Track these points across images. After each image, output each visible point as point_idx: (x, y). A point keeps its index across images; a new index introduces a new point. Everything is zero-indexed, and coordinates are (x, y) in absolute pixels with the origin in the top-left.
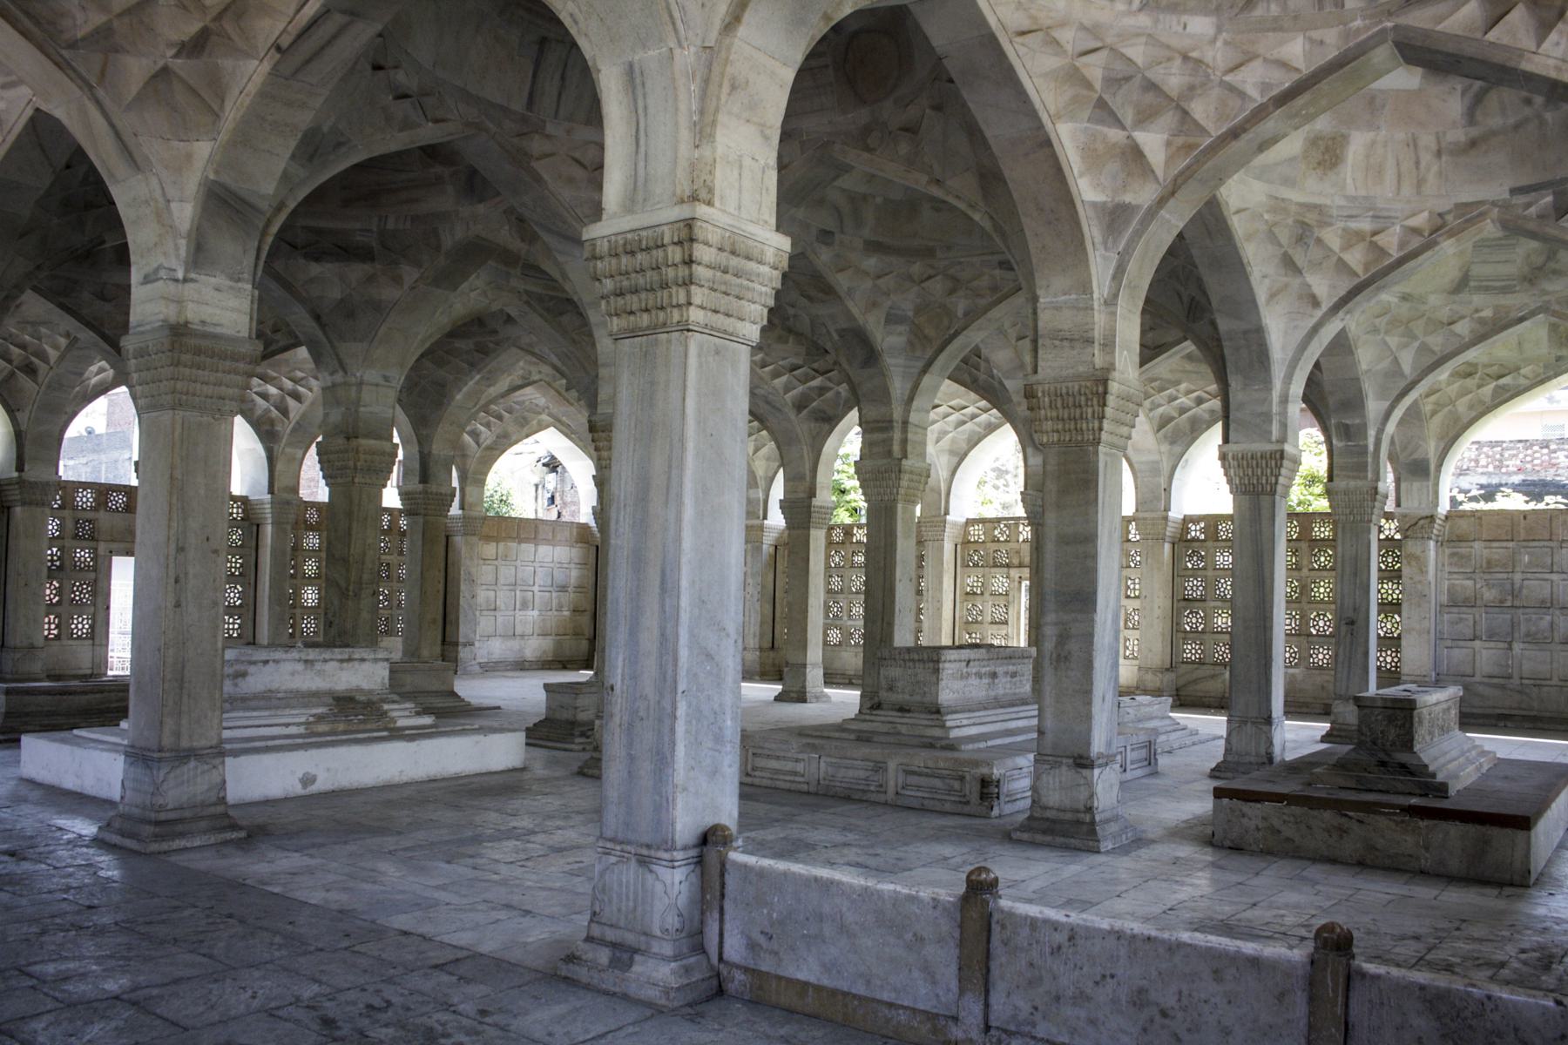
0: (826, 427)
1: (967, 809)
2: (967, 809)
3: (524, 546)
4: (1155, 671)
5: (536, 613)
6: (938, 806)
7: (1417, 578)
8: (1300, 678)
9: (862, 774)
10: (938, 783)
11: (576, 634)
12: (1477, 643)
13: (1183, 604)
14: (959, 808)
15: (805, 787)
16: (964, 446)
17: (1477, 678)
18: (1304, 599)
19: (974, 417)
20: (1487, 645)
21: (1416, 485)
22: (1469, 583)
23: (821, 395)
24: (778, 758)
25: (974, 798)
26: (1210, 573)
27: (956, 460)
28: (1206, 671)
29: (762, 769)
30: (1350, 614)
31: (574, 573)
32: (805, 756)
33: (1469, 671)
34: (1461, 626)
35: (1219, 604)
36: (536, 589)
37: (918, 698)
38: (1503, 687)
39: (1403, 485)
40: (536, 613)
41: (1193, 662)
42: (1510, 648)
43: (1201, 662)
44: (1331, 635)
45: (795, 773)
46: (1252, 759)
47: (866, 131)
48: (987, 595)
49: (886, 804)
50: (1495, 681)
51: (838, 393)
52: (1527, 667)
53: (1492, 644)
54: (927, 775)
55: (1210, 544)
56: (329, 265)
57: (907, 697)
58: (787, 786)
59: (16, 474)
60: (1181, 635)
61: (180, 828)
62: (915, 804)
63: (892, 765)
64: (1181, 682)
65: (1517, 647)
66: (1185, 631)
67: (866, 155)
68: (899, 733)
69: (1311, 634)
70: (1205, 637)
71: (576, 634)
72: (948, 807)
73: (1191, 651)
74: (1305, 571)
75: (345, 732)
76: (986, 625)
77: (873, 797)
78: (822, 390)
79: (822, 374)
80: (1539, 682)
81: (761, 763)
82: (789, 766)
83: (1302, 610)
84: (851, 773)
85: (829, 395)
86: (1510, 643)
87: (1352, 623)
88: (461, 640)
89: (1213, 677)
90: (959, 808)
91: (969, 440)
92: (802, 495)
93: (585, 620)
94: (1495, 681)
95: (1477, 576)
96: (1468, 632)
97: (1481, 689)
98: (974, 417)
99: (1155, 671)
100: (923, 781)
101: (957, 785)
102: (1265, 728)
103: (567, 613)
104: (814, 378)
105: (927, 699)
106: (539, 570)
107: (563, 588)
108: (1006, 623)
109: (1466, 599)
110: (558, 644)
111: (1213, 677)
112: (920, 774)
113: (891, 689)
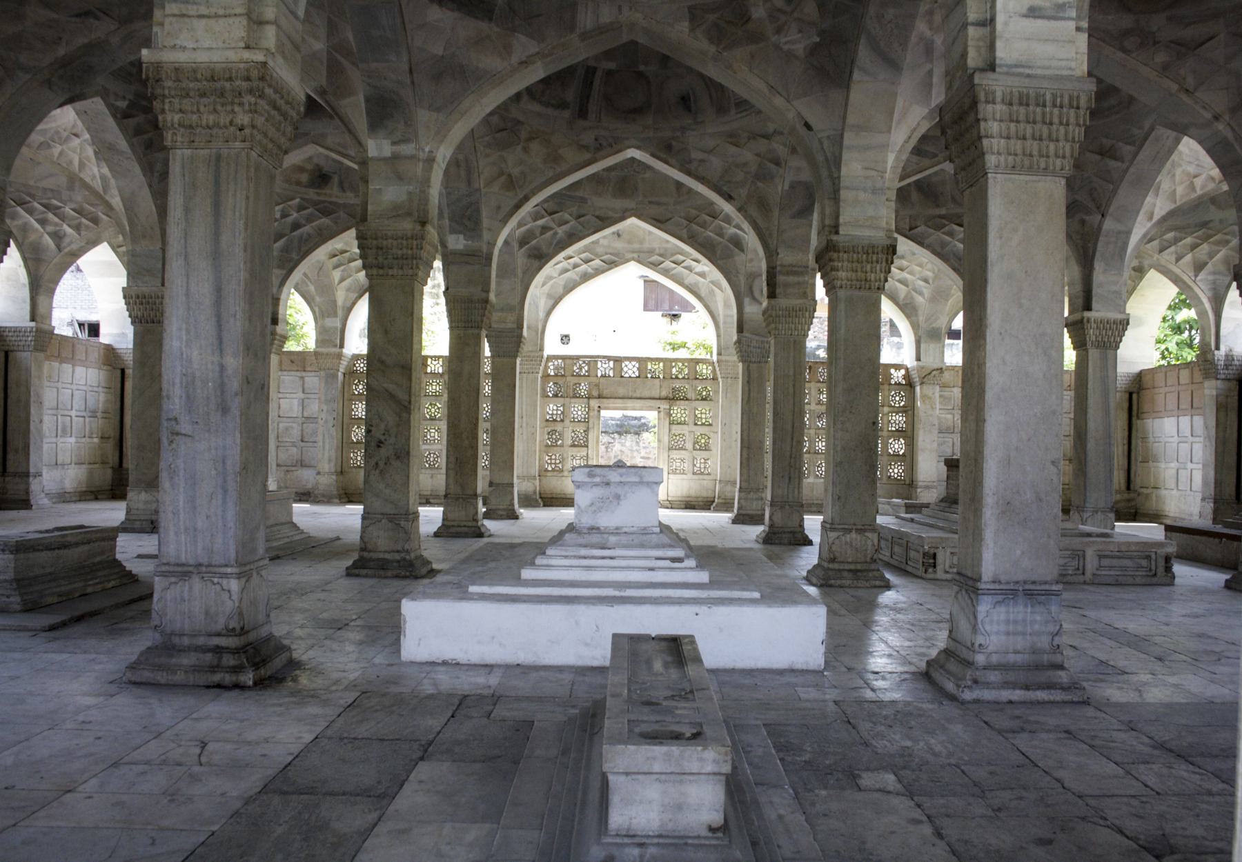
0: (536, 263)
1: (1155, 580)
3: (64, 365)
5: (73, 440)
6: (1130, 580)
11: (103, 463)
14: (1149, 581)
16: (561, 291)
19: (576, 266)
21: (932, 346)
22: (950, 416)
23: (542, 234)
25: (1161, 570)
27: (552, 302)
31: (102, 398)
36: (73, 413)
39: (923, 346)
40: (73, 440)
47: (1126, 33)
48: (567, 422)
51: (556, 234)
54: (1119, 558)
56: (449, 13)
59: (904, 245)
61: (1011, 677)
63: (1090, 553)
67: (1120, 54)
71: (103, 463)
72: (1138, 580)
76: (566, 448)
77: (1075, 579)
78: (545, 229)
79: (550, 214)
85: (549, 234)
88: (32, 470)
90: (1149, 581)
91: (565, 287)
92: (510, 325)
93: (110, 447)
98: (576, 266)
100: (1115, 562)
101: (1144, 563)
103: (96, 440)
104: (543, 217)
106: (76, 393)
107: (93, 414)
109: (948, 428)
110: (91, 474)
112: (1112, 557)
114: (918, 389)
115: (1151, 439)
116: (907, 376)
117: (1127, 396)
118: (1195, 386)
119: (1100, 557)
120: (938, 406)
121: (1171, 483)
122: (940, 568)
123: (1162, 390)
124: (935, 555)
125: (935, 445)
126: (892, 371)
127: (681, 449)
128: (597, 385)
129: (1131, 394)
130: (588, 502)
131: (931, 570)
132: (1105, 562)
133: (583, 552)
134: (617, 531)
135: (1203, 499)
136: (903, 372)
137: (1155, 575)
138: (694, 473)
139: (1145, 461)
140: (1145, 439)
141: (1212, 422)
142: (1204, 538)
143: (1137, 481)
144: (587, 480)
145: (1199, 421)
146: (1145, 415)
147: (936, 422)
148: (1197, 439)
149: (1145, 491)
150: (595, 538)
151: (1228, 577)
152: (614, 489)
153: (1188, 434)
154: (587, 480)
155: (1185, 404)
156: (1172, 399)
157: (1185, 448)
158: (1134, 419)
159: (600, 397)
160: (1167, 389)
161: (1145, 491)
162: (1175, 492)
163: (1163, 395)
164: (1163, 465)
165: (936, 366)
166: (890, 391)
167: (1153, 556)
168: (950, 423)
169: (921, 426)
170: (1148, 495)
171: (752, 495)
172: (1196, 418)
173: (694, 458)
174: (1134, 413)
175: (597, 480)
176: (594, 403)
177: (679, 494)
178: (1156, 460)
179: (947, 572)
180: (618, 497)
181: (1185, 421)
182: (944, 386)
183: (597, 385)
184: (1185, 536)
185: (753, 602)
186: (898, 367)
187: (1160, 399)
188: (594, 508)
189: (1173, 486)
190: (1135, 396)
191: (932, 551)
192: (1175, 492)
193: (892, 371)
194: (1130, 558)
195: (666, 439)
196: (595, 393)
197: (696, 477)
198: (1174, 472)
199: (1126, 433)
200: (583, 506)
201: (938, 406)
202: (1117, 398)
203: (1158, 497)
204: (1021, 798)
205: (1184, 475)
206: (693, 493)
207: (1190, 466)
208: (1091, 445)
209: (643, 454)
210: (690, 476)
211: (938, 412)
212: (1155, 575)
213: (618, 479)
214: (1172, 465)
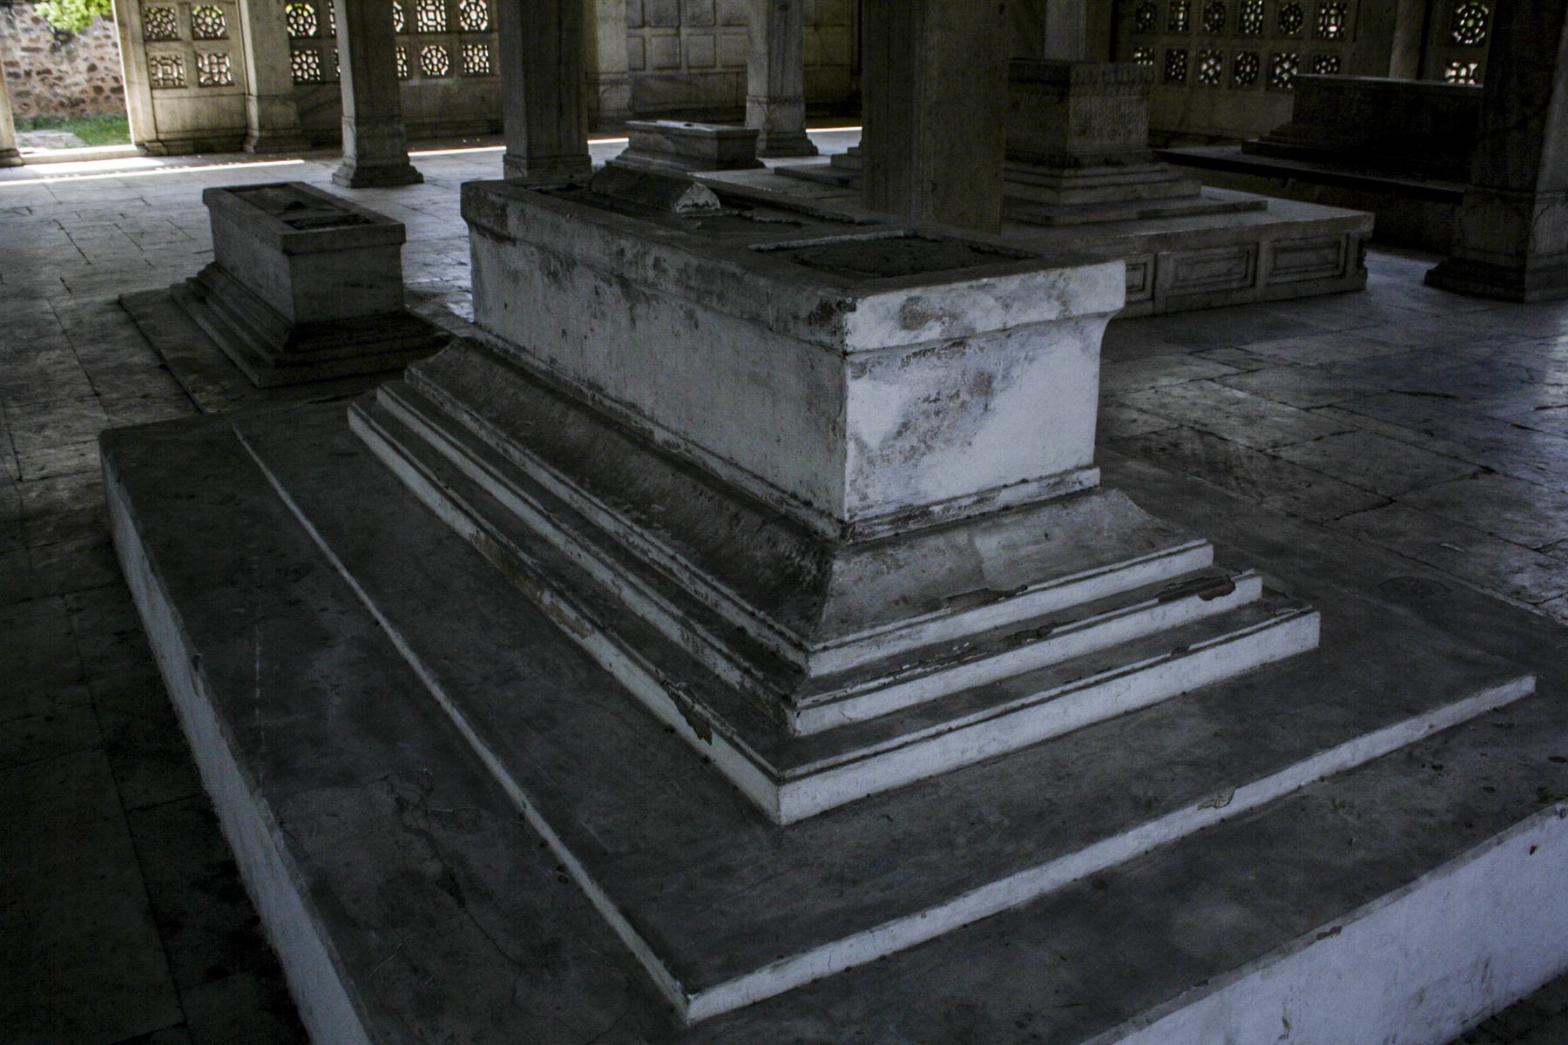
4: (285, 99)
8: (455, 89)
9: (1222, 267)
10: (1312, 257)
12: (647, 30)
17: (649, 72)
20: (656, 31)
38: (672, 79)
42: (678, 35)
44: (489, 30)
49: (1255, 303)
50: (665, 73)
52: (694, 53)
53: (661, 31)
54: (1301, 250)
63: (1265, 246)
65: (684, 31)
68: (1139, 200)
75: (1054, 572)
80: (705, 70)
86: (678, 28)
94: (665, 73)
97: (652, 83)
99: (285, 99)
101: (1330, 254)
113: (1083, 131)
127: (168, 38)
130: (888, 421)
132: (1285, 259)
133: (934, 631)
134: (985, 513)
137: (1344, 273)
138: (201, 85)
144: (901, 338)
150: (932, 560)
151: (1432, 266)
152: (976, 359)
154: (901, 338)
167: (1343, 243)
173: (197, 56)
175: (932, 332)
177: (178, 125)
180: (984, 385)
185: (1166, 660)
188: (910, 440)
194: (1315, 248)
195: (135, 21)
197: (206, 92)
200: (873, 442)
204: (890, 886)
206: (204, 122)
209: (25, 43)
210: (194, 90)
212: (1344, 273)
213: (995, 321)
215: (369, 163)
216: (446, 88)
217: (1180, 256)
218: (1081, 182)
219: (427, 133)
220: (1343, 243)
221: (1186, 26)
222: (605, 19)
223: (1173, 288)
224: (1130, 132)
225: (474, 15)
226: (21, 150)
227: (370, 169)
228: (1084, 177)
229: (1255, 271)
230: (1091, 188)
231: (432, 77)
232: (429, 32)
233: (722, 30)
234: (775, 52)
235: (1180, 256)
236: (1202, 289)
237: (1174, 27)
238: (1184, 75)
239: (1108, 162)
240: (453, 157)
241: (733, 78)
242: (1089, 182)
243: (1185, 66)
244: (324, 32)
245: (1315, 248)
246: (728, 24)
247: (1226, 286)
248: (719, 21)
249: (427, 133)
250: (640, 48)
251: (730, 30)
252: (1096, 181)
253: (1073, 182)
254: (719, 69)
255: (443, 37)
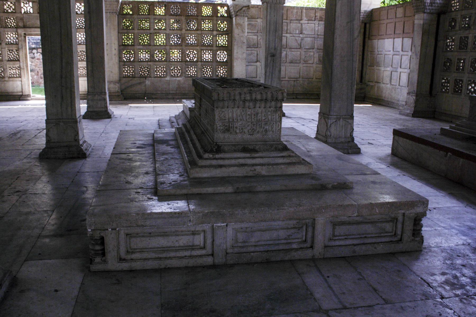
2: (399, 247)
6: (370, 250)
7: (241, 35)
8: (182, 81)
9: (282, 234)
10: (369, 229)
13: (122, 47)
15: (209, 260)
18: (184, 44)
22: (255, 37)
24: (165, 235)
25: (408, 235)
26: (136, 31)
28: (136, 81)
29: (142, 251)
30: (273, 51)
32: (207, 227)
33: (254, 75)
34: (252, 56)
35: (141, 47)
37: (258, 136)
41: (129, 77)
43: (133, 77)
45: (192, 247)
46: (343, 140)
54: (358, 223)
55: (135, 16)
57: (246, 137)
58: (184, 263)
60: (123, 63)
62: (346, 252)
63: (321, 221)
64: (123, 87)
66: (124, 61)
69: (187, 61)
70: (136, 64)
72: (380, 249)
73: (128, 71)
74: (184, 30)
76: (5, 62)
81: (138, 243)
82: (184, 240)
83: (182, 49)
84: (267, 236)
87: (273, 56)
89: (140, 83)
95: (259, 34)
96: (255, 59)
100: (353, 229)
101: (388, 227)
102: (350, 121)
105: (270, 135)
108: (19, 60)
111: (140, 83)
112: (349, 223)
113: (227, 130)
114: (234, 19)
115: (376, 52)
116: (228, 11)
117: (363, 25)
118: (406, 19)
119: (335, 225)
120: (246, 31)
121: (387, 80)
122: (111, 255)
123: (385, 22)
124: (102, 239)
125: (245, 55)
126: (219, 8)
128: (22, 19)
129: (365, 24)
131: (98, 260)
132: (340, 230)
135: (409, 93)
136: (226, 8)
137: (401, 240)
139: (372, 65)
140: (372, 52)
141: (418, 42)
142: (430, 149)
143: (367, 77)
145: (408, 42)
146: (373, 37)
147: (245, 41)
148: (406, 53)
149: (371, 84)
153: (400, 50)
155: (399, 30)
156: (391, 26)
157: (397, 58)
158: (367, 39)
159: (25, 27)
160: (388, 21)
161: (371, 84)
162: (389, 86)
163: (386, 25)
164: (382, 69)
165: (245, 5)
166: (217, 21)
167: (400, 218)
168: (255, 41)
169: (236, 43)
170: (372, 86)
171: (96, 97)
172: (406, 40)
174: (367, 36)
176: (21, 31)
178: (378, 65)
179: (121, 260)
181: (398, 41)
182: (251, 18)
183: (22, 19)
184: (411, 142)
186: (222, 5)
187: (383, 28)
189: (388, 82)
190: (368, 25)
191: (97, 235)
192: (389, 86)
193: (219, 8)
194: (373, 223)
196: (21, 24)
198: (389, 73)
199: (362, 48)
201: (246, 31)
202: (357, 25)
203: (379, 88)
205: (395, 75)
207: (399, 70)
208: (337, 61)
211: (246, 34)
212: (401, 240)
214: (388, 69)
215: (91, 110)
216: (179, 81)
217: (238, 226)
218: (214, 162)
219: (170, 97)
220: (400, 218)
221: (463, 69)
222: (237, 59)
223: (233, 247)
224: (266, 131)
225: (191, 56)
226: (32, 95)
227: (91, 112)
228: (217, 159)
229: (313, 237)
230: (221, 166)
231: (174, 77)
232: (174, 61)
233: (289, 64)
234: (268, 74)
235: (238, 226)
236: (262, 249)
237: (458, 69)
238: (461, 90)
239: (245, 150)
240: (137, 107)
241: (293, 83)
242: (221, 162)
243: (462, 87)
244: (136, 60)
245: (373, 223)
246: (291, 62)
247: (286, 247)
248: (288, 61)
249: (170, 97)
250: (255, 70)
251: (292, 64)
252: (227, 162)
253: (208, 162)
254: (287, 79)
255: (179, 63)
